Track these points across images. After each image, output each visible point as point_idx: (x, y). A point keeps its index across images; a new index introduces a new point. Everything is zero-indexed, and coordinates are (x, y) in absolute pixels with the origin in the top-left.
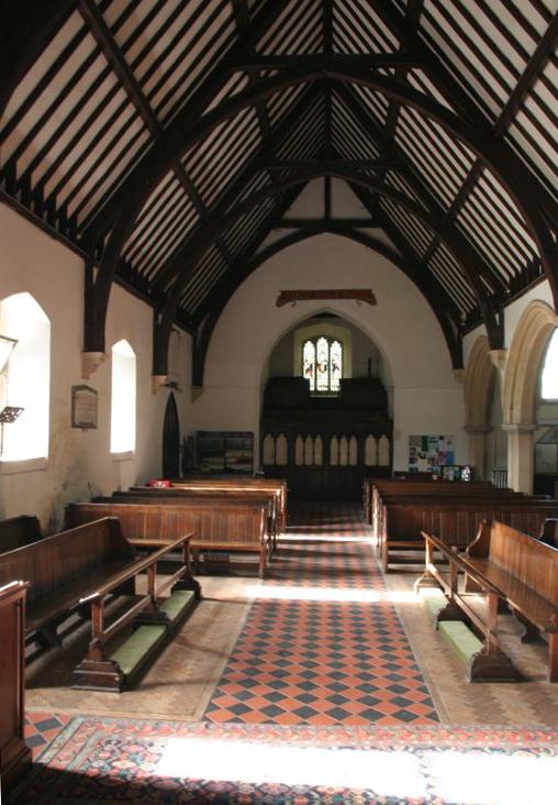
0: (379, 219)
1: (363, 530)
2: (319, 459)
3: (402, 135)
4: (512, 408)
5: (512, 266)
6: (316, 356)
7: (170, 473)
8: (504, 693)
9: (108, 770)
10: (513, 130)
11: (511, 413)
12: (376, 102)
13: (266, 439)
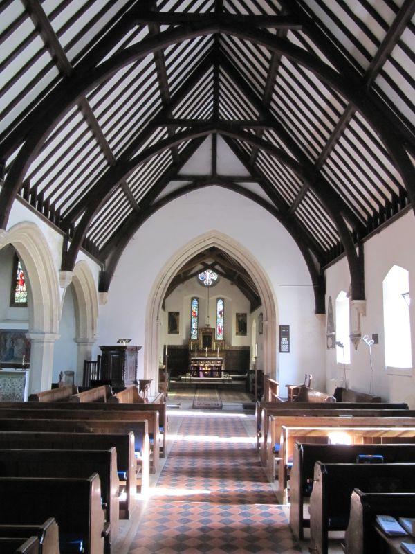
0: (256, 175)
3: (261, 157)
10: (380, 81)
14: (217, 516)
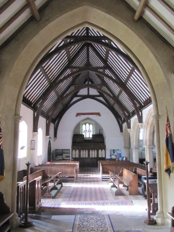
0: (101, 95)
1: (98, 173)
2: (87, 156)
4: (133, 143)
5: (143, 99)
6: (86, 128)
7: (49, 160)
8: (121, 198)
9: (54, 207)
11: (134, 144)
12: (102, 50)
13: (73, 151)
14: (89, 175)
